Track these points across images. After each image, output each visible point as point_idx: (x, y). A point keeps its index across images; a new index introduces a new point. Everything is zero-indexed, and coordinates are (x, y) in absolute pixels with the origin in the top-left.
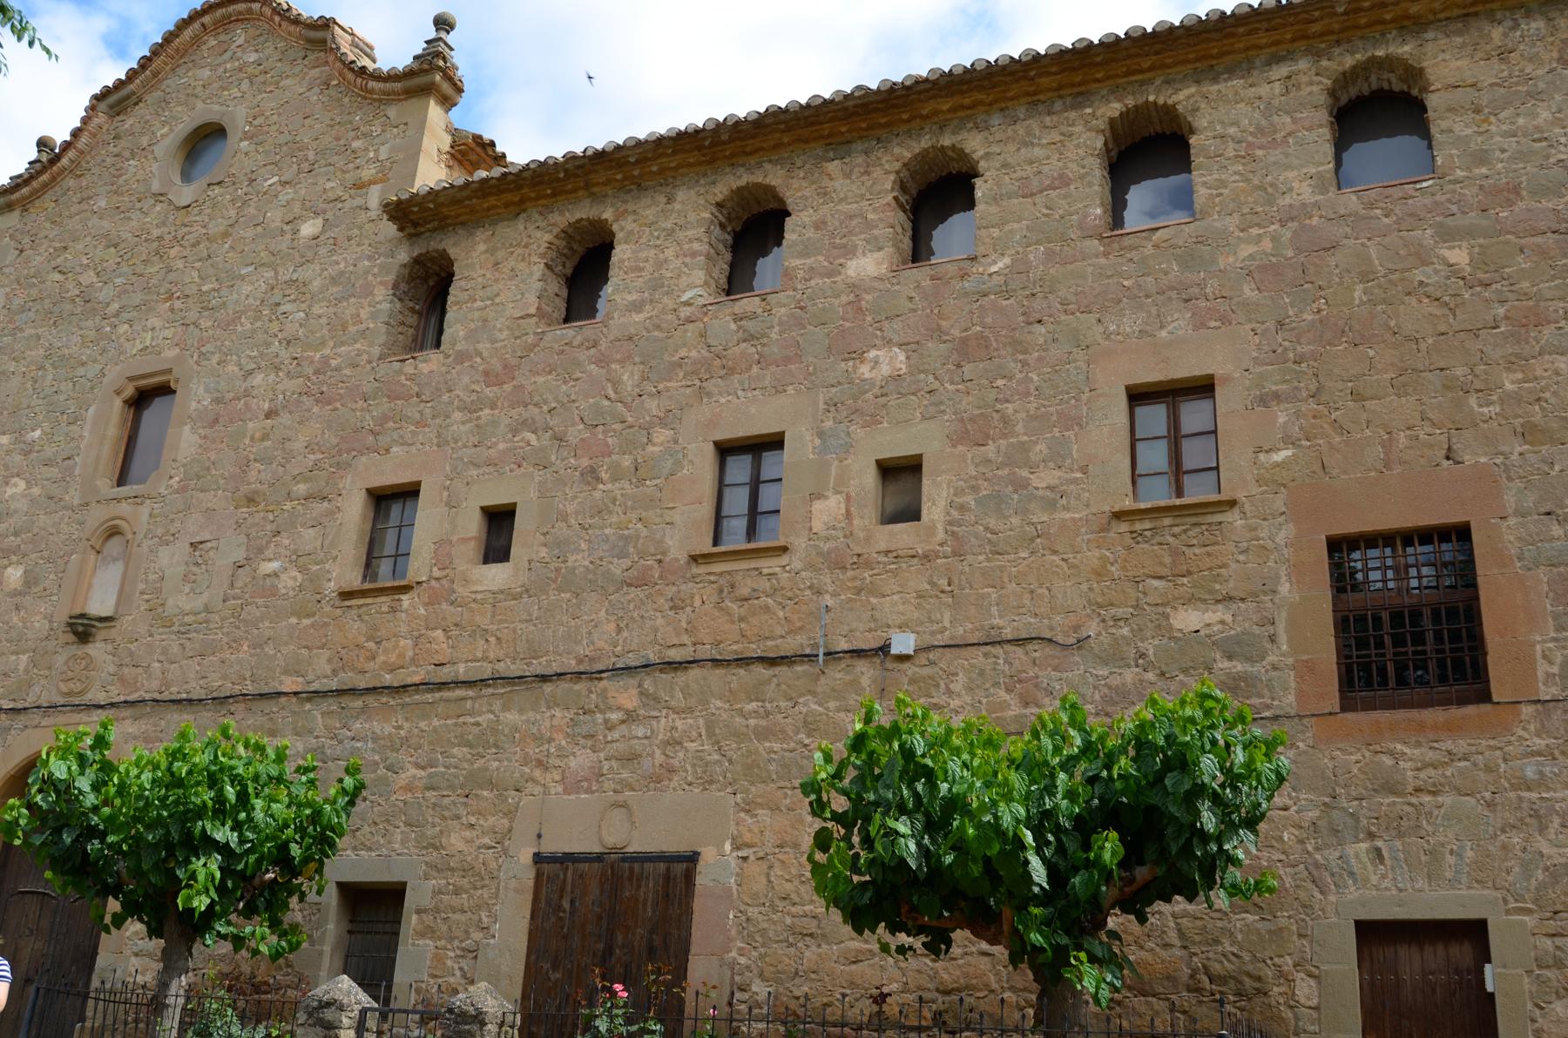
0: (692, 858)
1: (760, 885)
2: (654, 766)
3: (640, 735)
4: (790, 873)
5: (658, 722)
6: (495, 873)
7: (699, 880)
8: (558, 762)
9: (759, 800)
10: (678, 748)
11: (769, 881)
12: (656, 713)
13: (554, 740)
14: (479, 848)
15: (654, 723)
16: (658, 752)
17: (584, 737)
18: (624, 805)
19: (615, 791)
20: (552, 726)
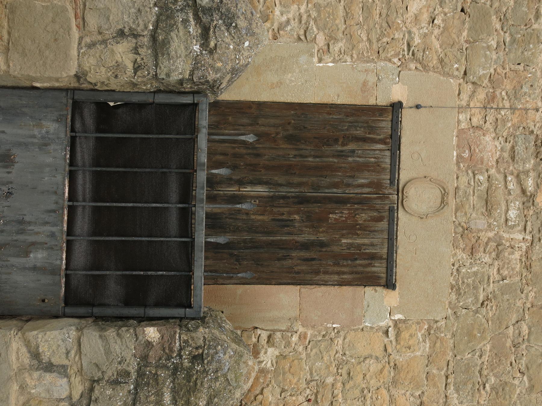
0: (390, 285)
1: (362, 349)
2: (479, 231)
3: (510, 212)
4: (371, 378)
5: (520, 232)
6: (383, 55)
7: (369, 290)
8: (490, 119)
9: (438, 345)
10: (494, 255)
11: (365, 358)
12: (529, 228)
13: (513, 113)
14: (410, 32)
15: (520, 228)
16: (491, 234)
17: (513, 147)
18: (443, 202)
19: (457, 188)
20: (527, 110)
